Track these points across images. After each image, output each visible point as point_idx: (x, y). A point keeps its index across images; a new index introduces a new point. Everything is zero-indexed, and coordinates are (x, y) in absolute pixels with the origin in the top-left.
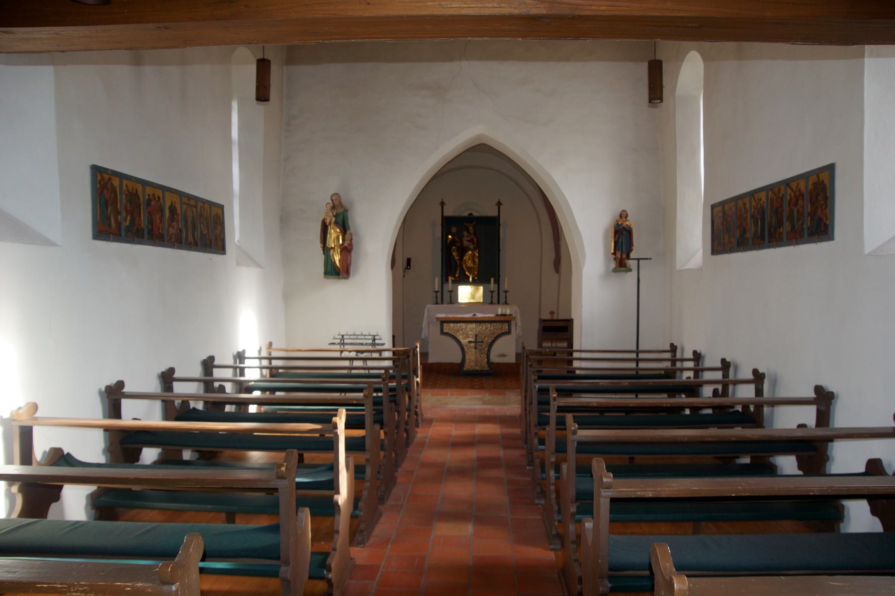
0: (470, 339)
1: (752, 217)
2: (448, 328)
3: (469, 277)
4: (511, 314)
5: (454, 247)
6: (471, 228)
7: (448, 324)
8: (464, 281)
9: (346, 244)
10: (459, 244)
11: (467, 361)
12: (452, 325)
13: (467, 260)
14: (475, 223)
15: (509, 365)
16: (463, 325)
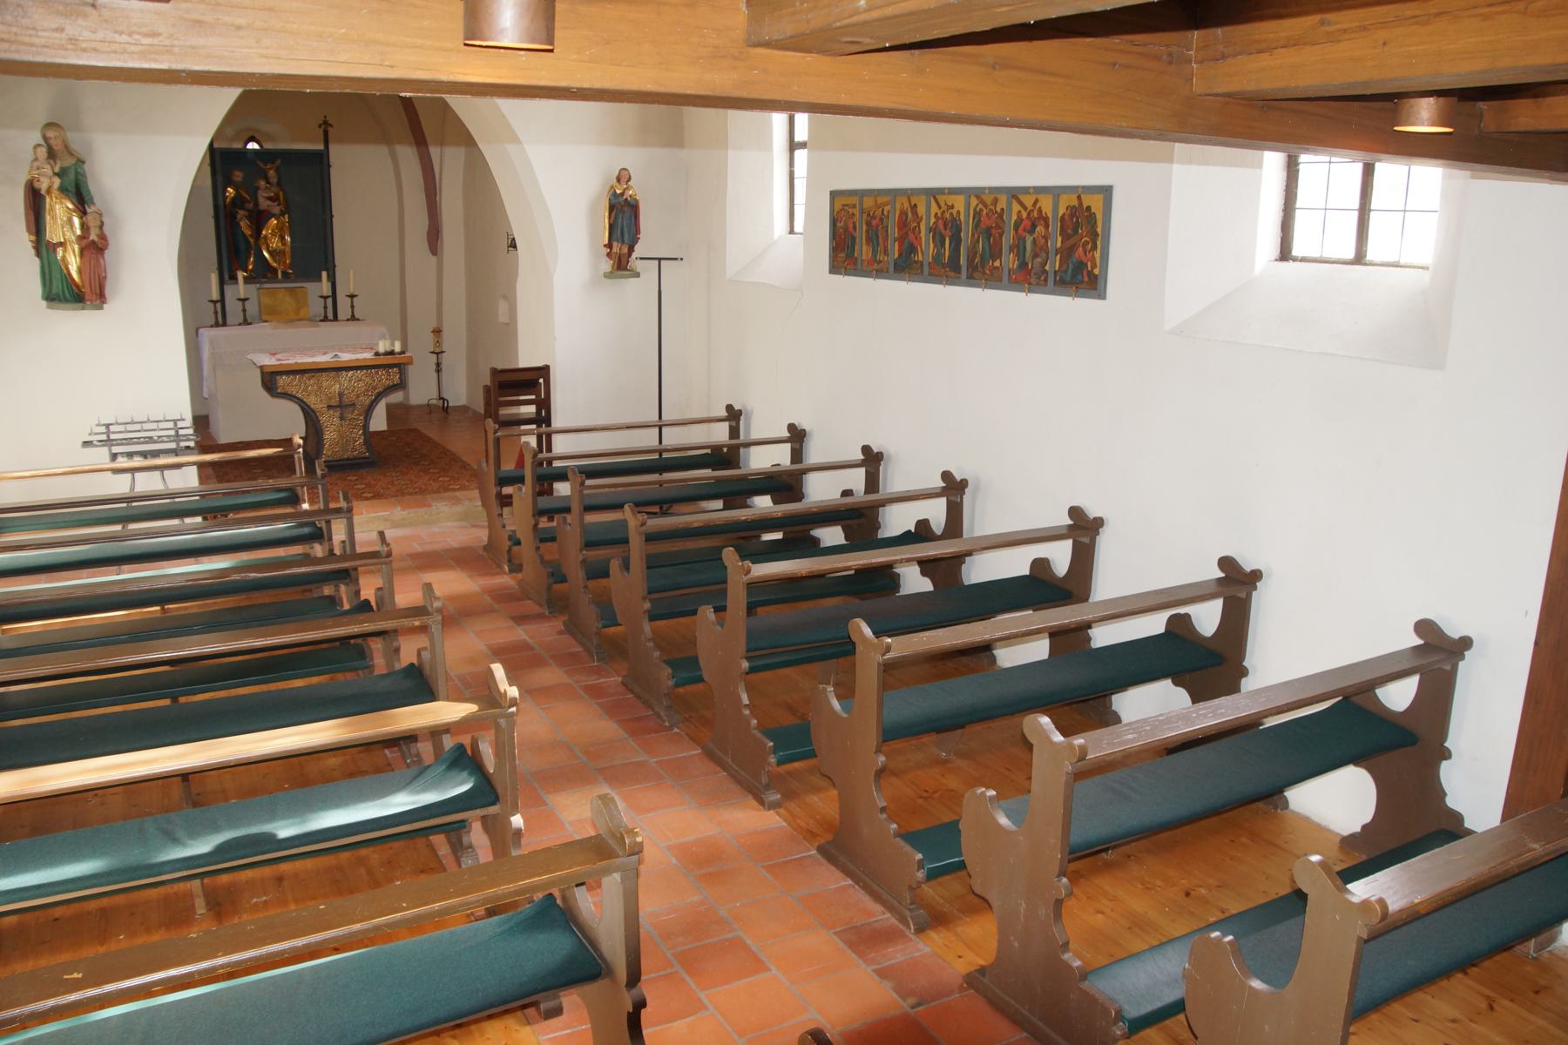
1: (932, 230)
6: (272, 173)
9: (93, 236)
10: (250, 206)
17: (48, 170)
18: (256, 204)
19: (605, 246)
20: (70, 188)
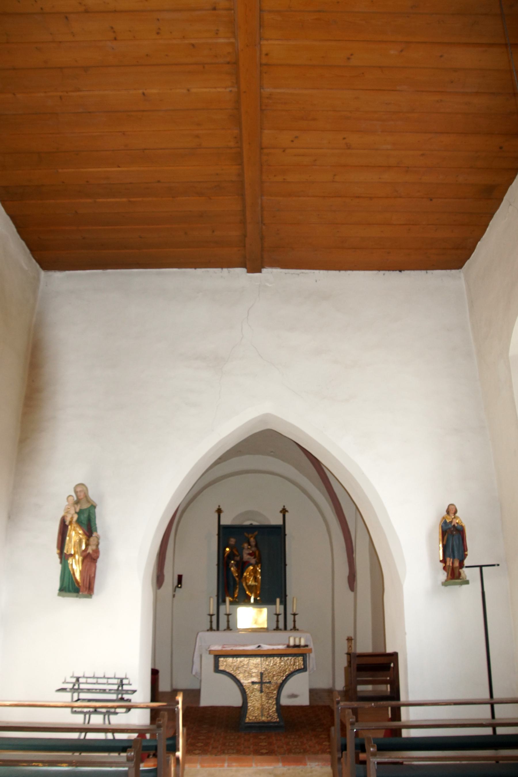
0: (255, 679)
2: (225, 663)
3: (250, 598)
4: (306, 644)
5: (232, 562)
6: (252, 540)
7: (225, 659)
8: (244, 600)
9: (90, 551)
11: (250, 708)
12: (230, 660)
13: (248, 576)
14: (256, 533)
15: (301, 708)
16: (245, 660)
17: (73, 508)
18: (242, 558)
19: (441, 561)
20: (83, 522)
